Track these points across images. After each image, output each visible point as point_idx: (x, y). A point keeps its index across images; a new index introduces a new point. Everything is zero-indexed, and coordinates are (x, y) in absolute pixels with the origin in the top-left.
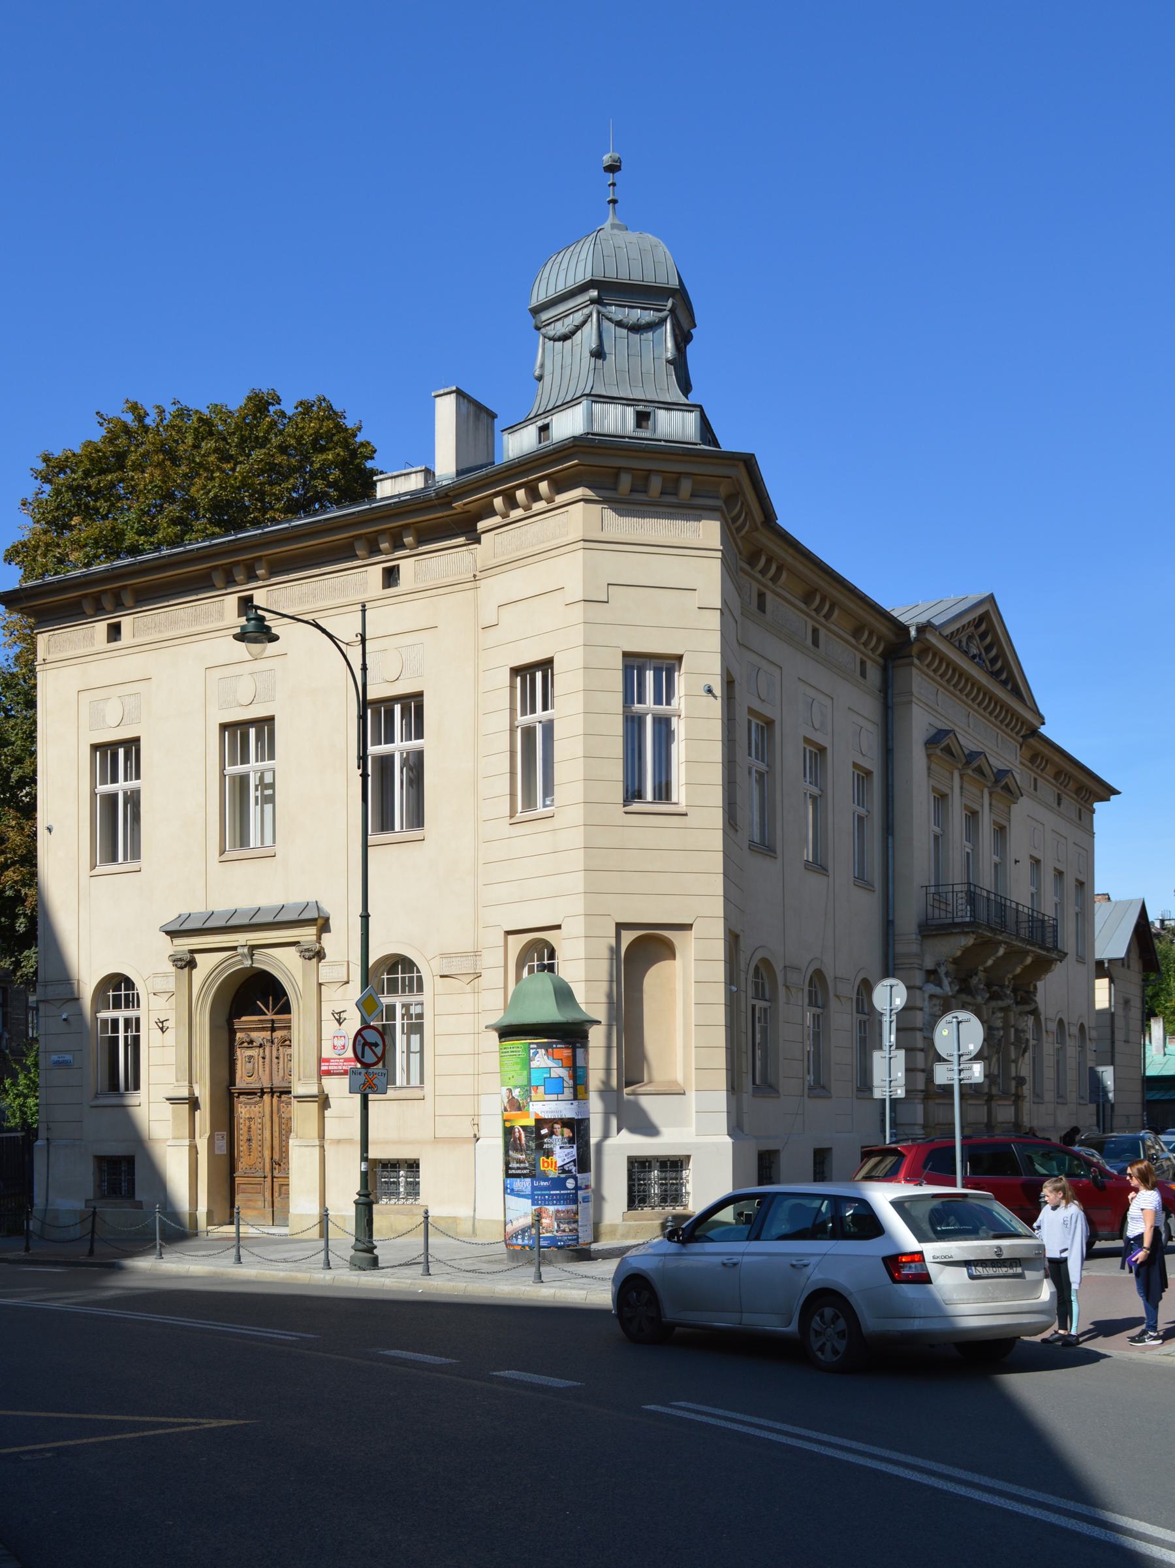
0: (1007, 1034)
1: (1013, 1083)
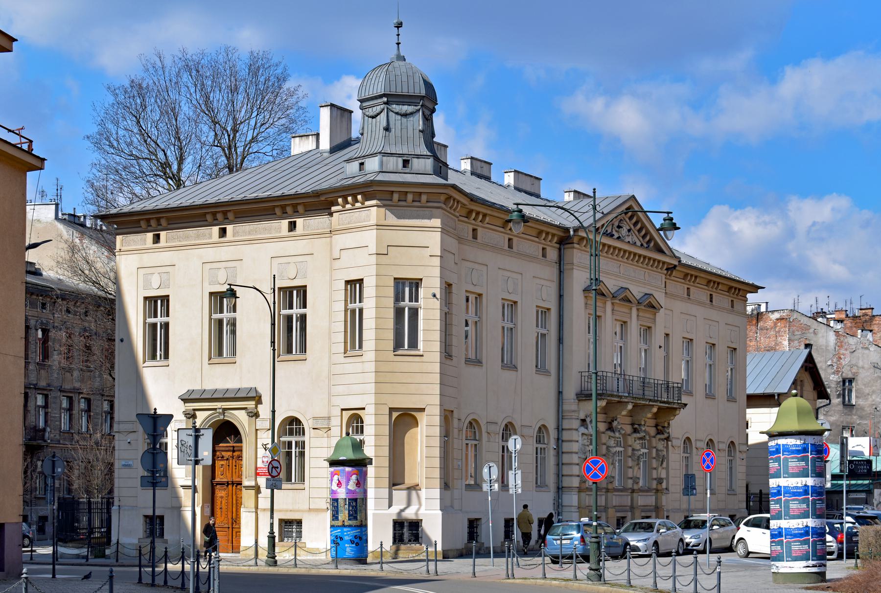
1: (655, 482)
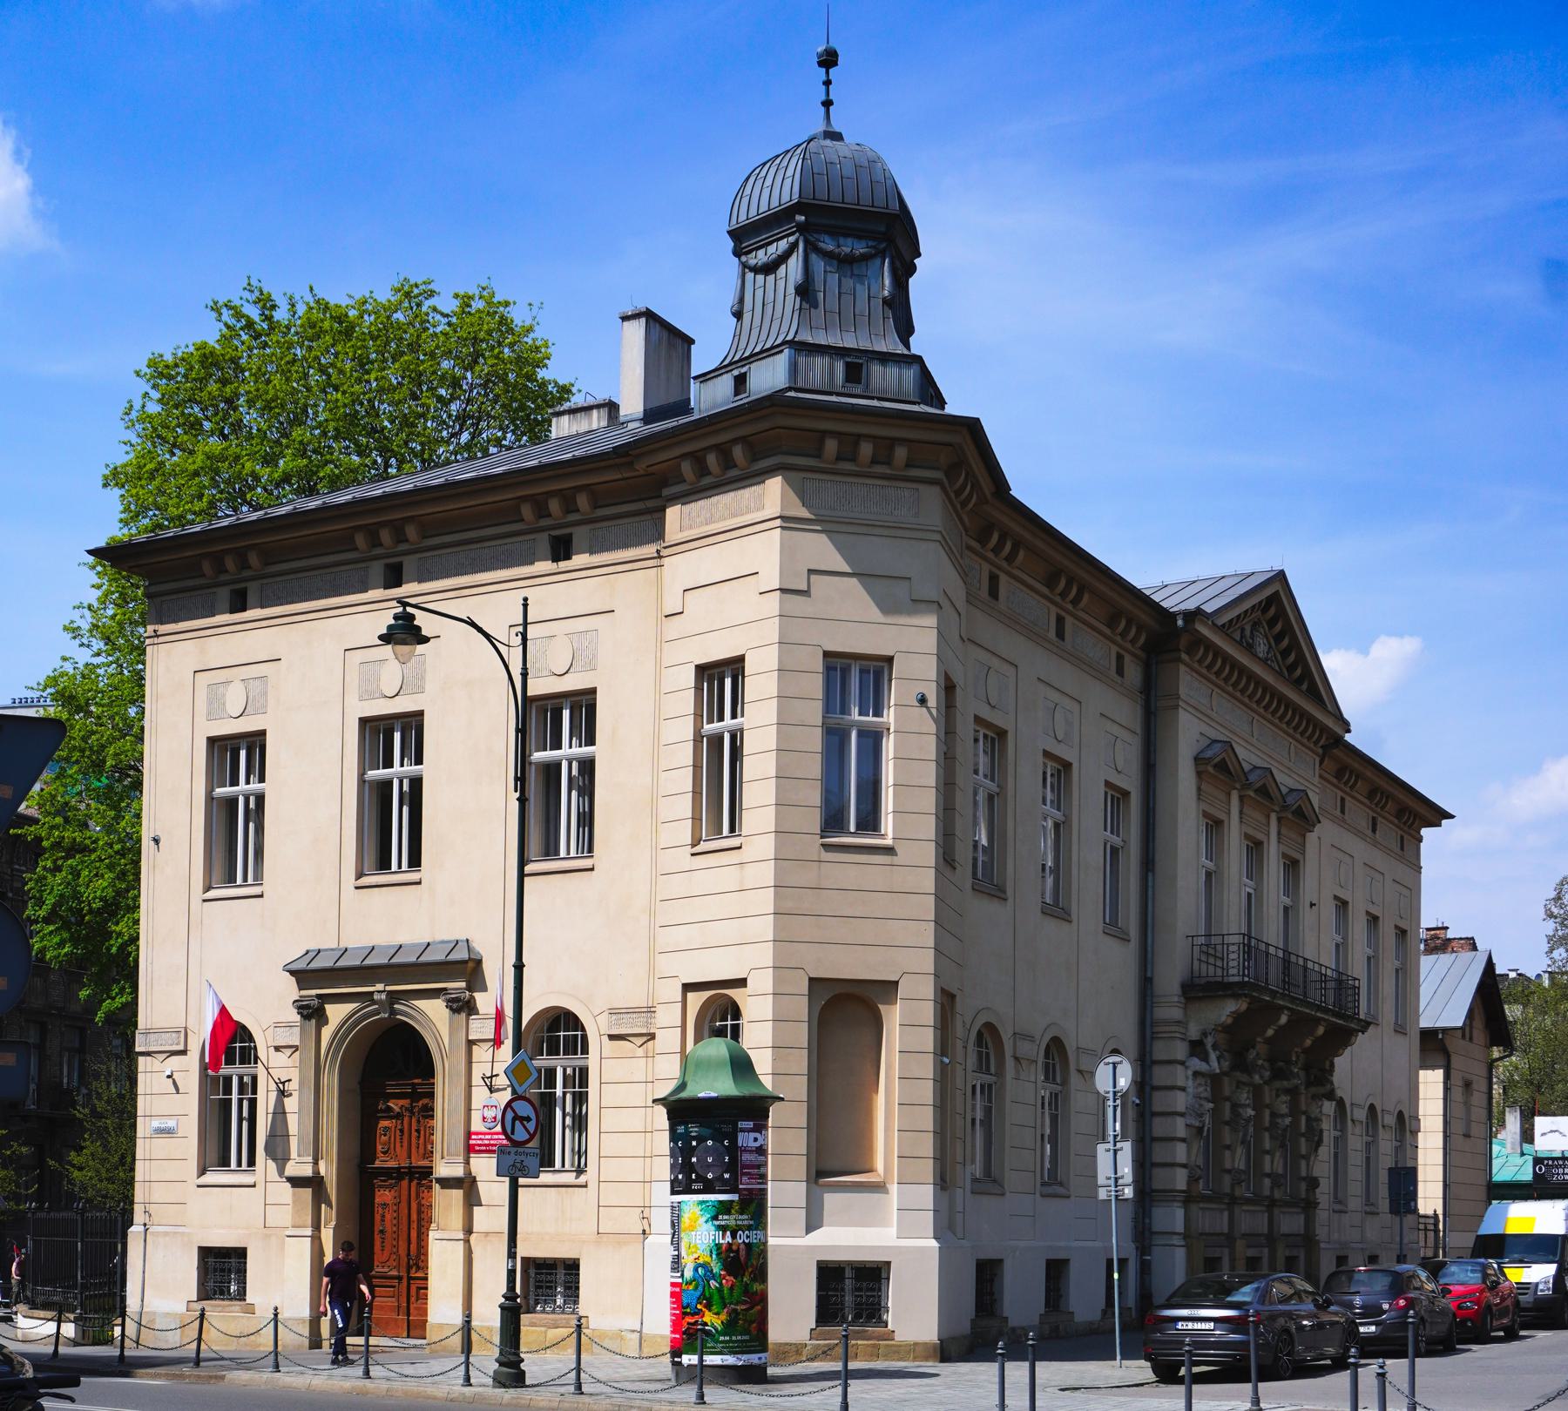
0: (1295, 1123)
1: (1303, 1186)
